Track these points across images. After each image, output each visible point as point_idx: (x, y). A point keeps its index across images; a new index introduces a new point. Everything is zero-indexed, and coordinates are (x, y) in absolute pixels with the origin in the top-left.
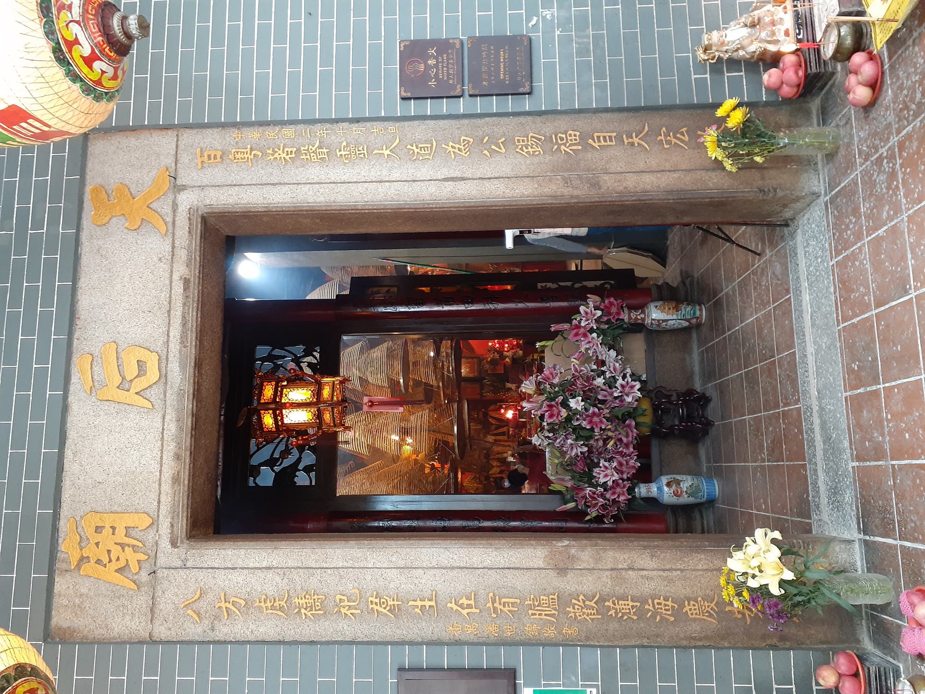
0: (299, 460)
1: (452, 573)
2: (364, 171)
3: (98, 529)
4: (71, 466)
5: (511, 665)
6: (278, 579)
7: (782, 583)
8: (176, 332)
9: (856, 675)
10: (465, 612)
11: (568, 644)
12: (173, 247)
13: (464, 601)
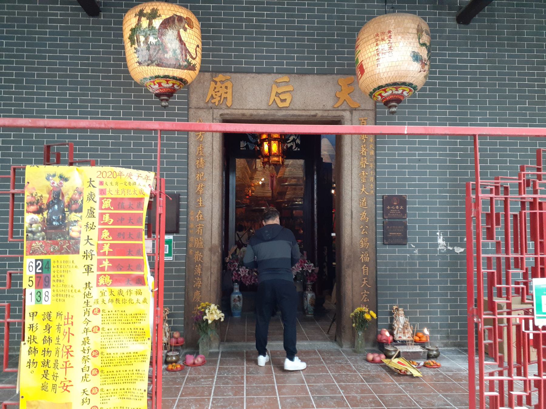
0: (251, 142)
1: (210, 212)
2: (356, 182)
3: (226, 87)
4: (248, 77)
5: (180, 232)
6: (209, 152)
7: (207, 320)
8: (297, 113)
9: (177, 343)
10: (197, 216)
11: (187, 251)
12: (329, 110)
13: (201, 216)
